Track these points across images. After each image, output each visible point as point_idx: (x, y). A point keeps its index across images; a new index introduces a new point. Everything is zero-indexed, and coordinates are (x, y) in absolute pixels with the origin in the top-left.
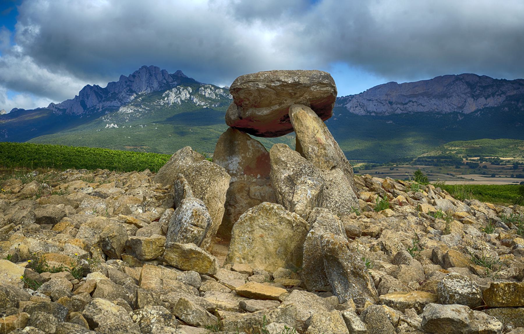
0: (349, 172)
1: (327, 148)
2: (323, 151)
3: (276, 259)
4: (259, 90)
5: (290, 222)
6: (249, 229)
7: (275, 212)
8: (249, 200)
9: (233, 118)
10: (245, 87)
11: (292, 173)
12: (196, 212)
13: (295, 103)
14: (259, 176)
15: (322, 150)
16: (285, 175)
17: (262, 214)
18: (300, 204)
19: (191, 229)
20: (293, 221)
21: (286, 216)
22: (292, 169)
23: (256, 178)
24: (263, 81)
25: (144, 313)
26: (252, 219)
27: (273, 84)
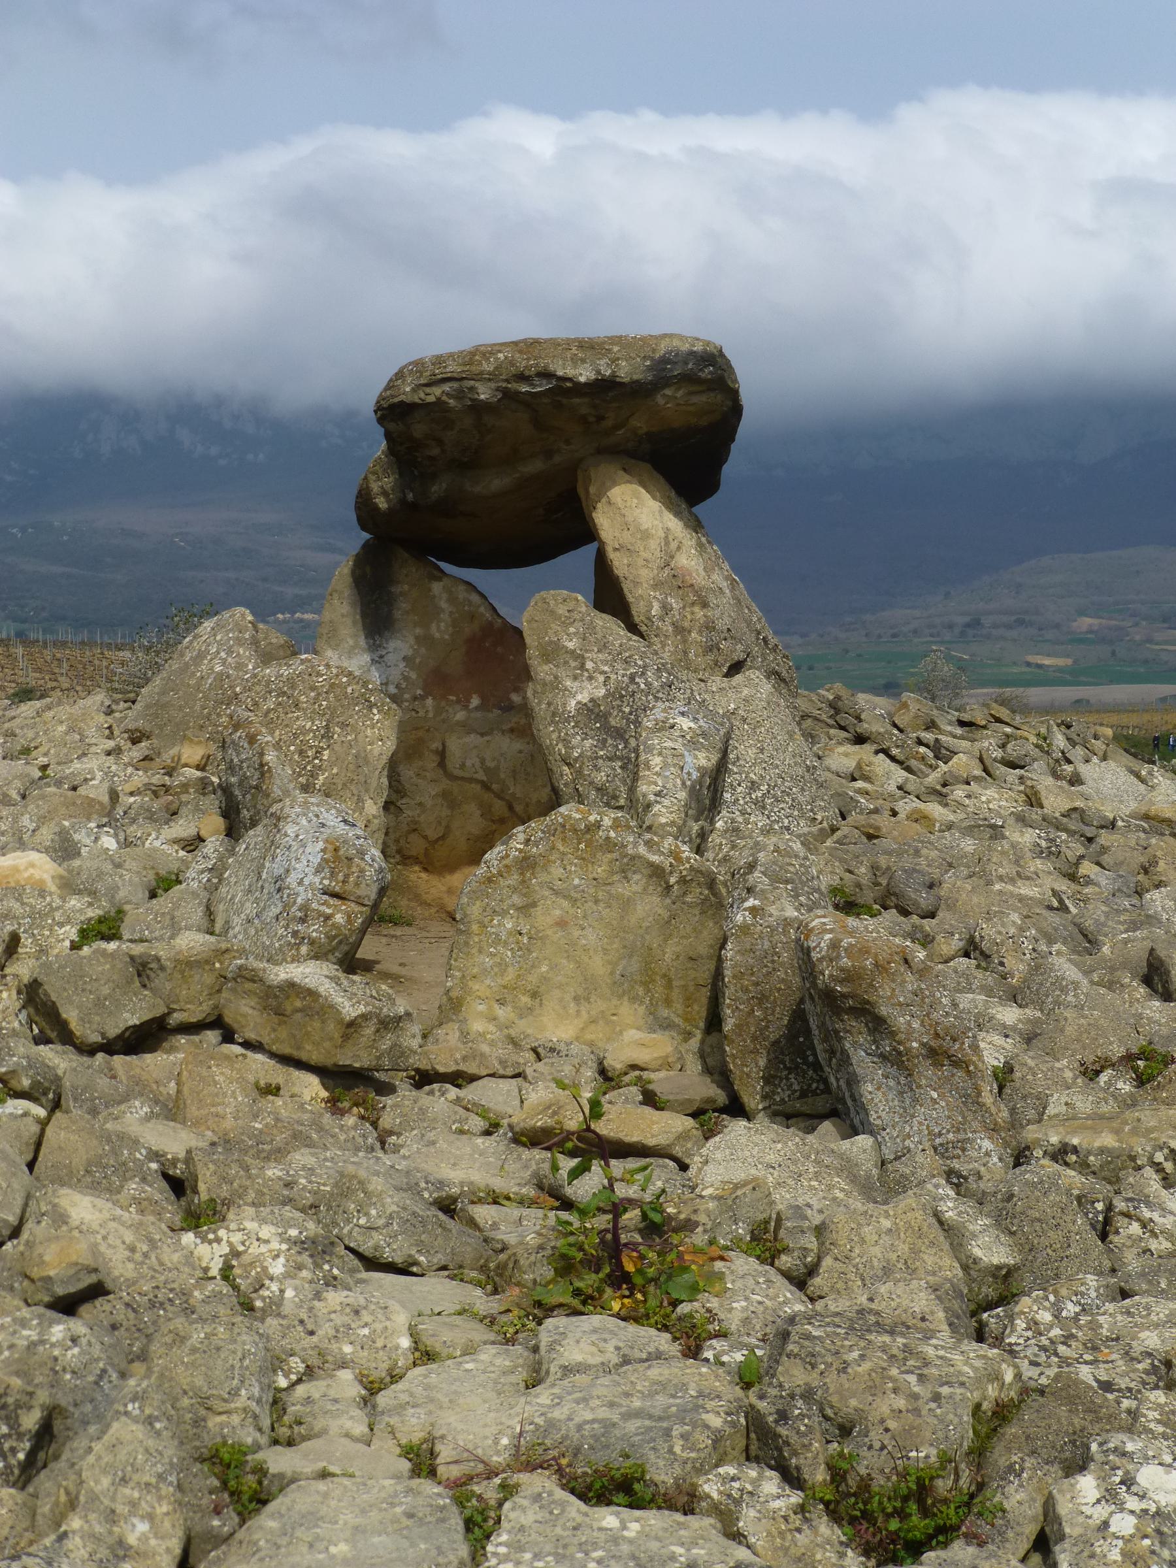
0: (783, 680)
1: (713, 601)
2: (699, 613)
3: (615, 1002)
4: (478, 408)
5: (657, 873)
6: (516, 899)
7: (608, 838)
8: (445, 784)
9: (382, 503)
10: (431, 399)
11: (602, 692)
12: (336, 850)
13: (600, 451)
14: (475, 701)
15: (696, 609)
16: (579, 697)
17: (560, 846)
18: (666, 802)
19: (322, 908)
20: (668, 869)
21: (642, 850)
22: (601, 678)
23: (466, 707)
24: (492, 377)
25: (236, 1238)
26: (526, 864)
27: (525, 388)
